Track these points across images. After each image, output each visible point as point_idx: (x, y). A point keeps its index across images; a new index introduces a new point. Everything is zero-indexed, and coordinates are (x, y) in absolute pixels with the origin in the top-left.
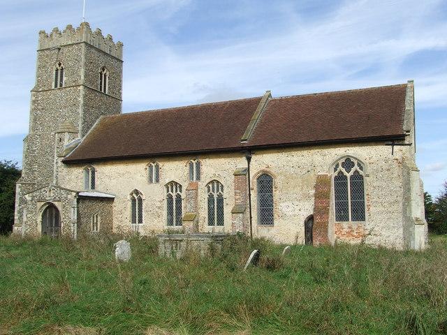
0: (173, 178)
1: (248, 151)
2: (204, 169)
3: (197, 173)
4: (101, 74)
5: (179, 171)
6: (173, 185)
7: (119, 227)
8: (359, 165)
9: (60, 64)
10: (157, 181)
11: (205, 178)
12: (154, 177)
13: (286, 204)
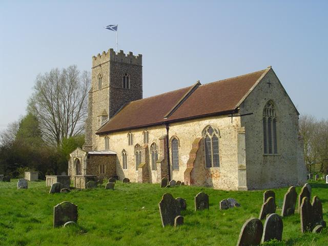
1: (167, 124)
2: (150, 136)
3: (146, 138)
4: (124, 77)
9: (126, 75)
10: (132, 144)
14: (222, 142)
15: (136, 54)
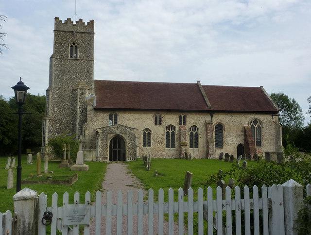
1: (211, 113)
3: (183, 121)
6: (170, 127)
10: (160, 124)
15: (86, 21)
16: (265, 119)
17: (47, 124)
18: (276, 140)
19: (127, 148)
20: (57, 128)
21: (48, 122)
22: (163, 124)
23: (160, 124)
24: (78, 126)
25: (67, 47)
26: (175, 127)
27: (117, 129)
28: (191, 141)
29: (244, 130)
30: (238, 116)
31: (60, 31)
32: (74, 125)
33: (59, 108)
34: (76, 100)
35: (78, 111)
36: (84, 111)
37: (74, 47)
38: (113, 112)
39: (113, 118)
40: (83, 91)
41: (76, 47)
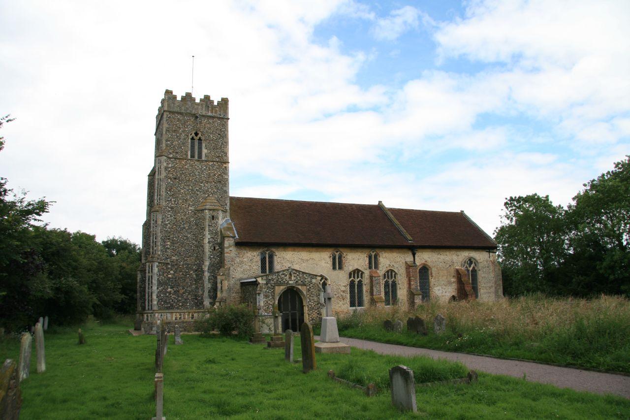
0: (356, 267)
1: (412, 249)
3: (373, 263)
5: (361, 261)
6: (357, 272)
7: (439, 303)
8: (475, 263)
9: (196, 134)
10: (340, 268)
11: (382, 271)
12: (338, 264)
13: (438, 288)
14: (481, 275)
15: (216, 99)
16: (481, 257)
17: (156, 270)
18: (495, 288)
19: (306, 309)
20: (170, 278)
21: (157, 266)
22: (345, 268)
23: (340, 268)
24: (207, 274)
25: (185, 139)
26: (363, 273)
27: (290, 278)
28: (386, 293)
29: (458, 274)
30: (448, 253)
31: (173, 113)
32: (200, 271)
33: (173, 243)
34: (203, 229)
35: (207, 248)
36: (219, 248)
37: (197, 139)
38: (266, 249)
39: (396, 222)
40: (215, 214)
41: (200, 139)
